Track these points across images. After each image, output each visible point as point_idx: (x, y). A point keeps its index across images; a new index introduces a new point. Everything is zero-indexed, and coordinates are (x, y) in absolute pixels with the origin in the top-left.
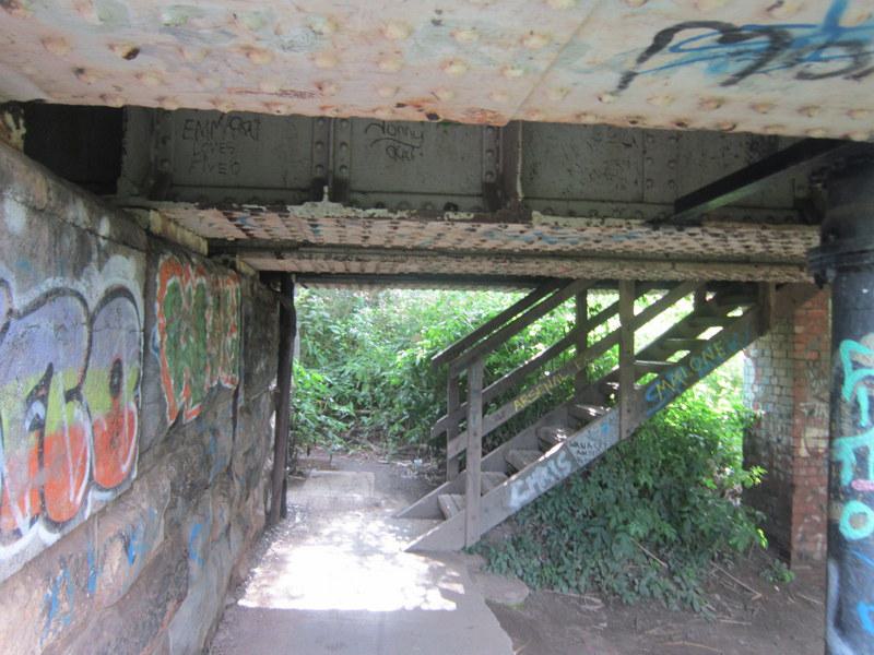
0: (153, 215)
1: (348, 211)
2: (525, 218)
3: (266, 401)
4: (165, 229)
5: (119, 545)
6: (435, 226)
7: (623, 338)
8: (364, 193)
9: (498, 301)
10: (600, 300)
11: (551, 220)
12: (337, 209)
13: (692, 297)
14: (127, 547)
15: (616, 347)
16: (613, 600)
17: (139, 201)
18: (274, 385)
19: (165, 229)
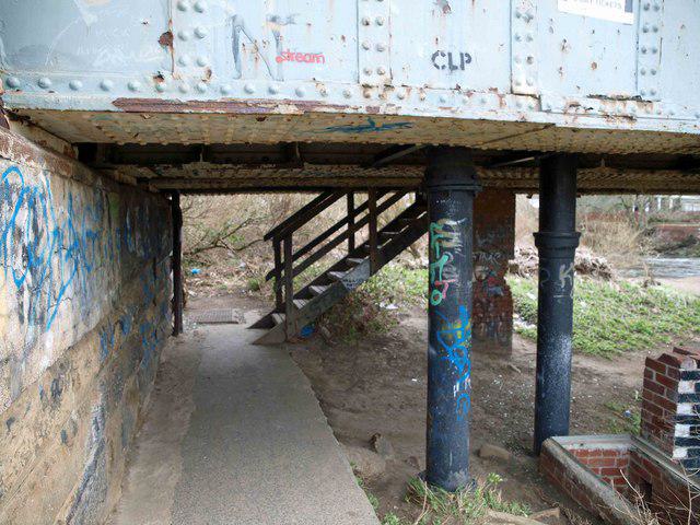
0: (116, 172)
1: (212, 166)
2: (300, 166)
3: (168, 262)
4: (95, 178)
5: (118, 325)
6: (257, 171)
7: (352, 212)
8: (219, 153)
9: (302, 199)
10: (361, 198)
11: (313, 166)
12: (208, 165)
13: (345, 196)
14: (122, 327)
15: (355, 207)
16: (326, 343)
17: (108, 165)
18: (171, 254)
19: (95, 178)
